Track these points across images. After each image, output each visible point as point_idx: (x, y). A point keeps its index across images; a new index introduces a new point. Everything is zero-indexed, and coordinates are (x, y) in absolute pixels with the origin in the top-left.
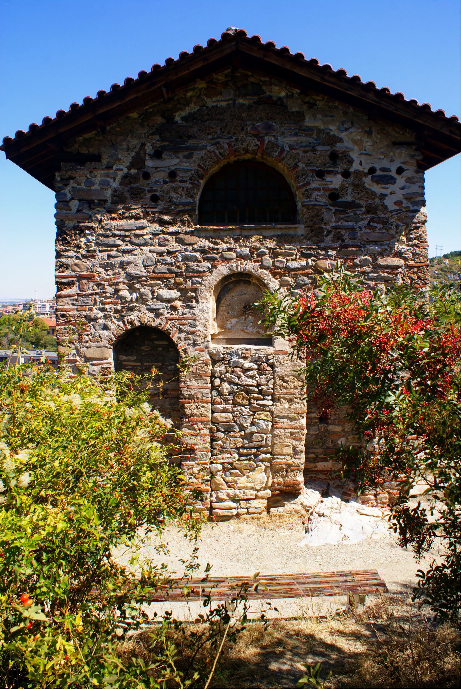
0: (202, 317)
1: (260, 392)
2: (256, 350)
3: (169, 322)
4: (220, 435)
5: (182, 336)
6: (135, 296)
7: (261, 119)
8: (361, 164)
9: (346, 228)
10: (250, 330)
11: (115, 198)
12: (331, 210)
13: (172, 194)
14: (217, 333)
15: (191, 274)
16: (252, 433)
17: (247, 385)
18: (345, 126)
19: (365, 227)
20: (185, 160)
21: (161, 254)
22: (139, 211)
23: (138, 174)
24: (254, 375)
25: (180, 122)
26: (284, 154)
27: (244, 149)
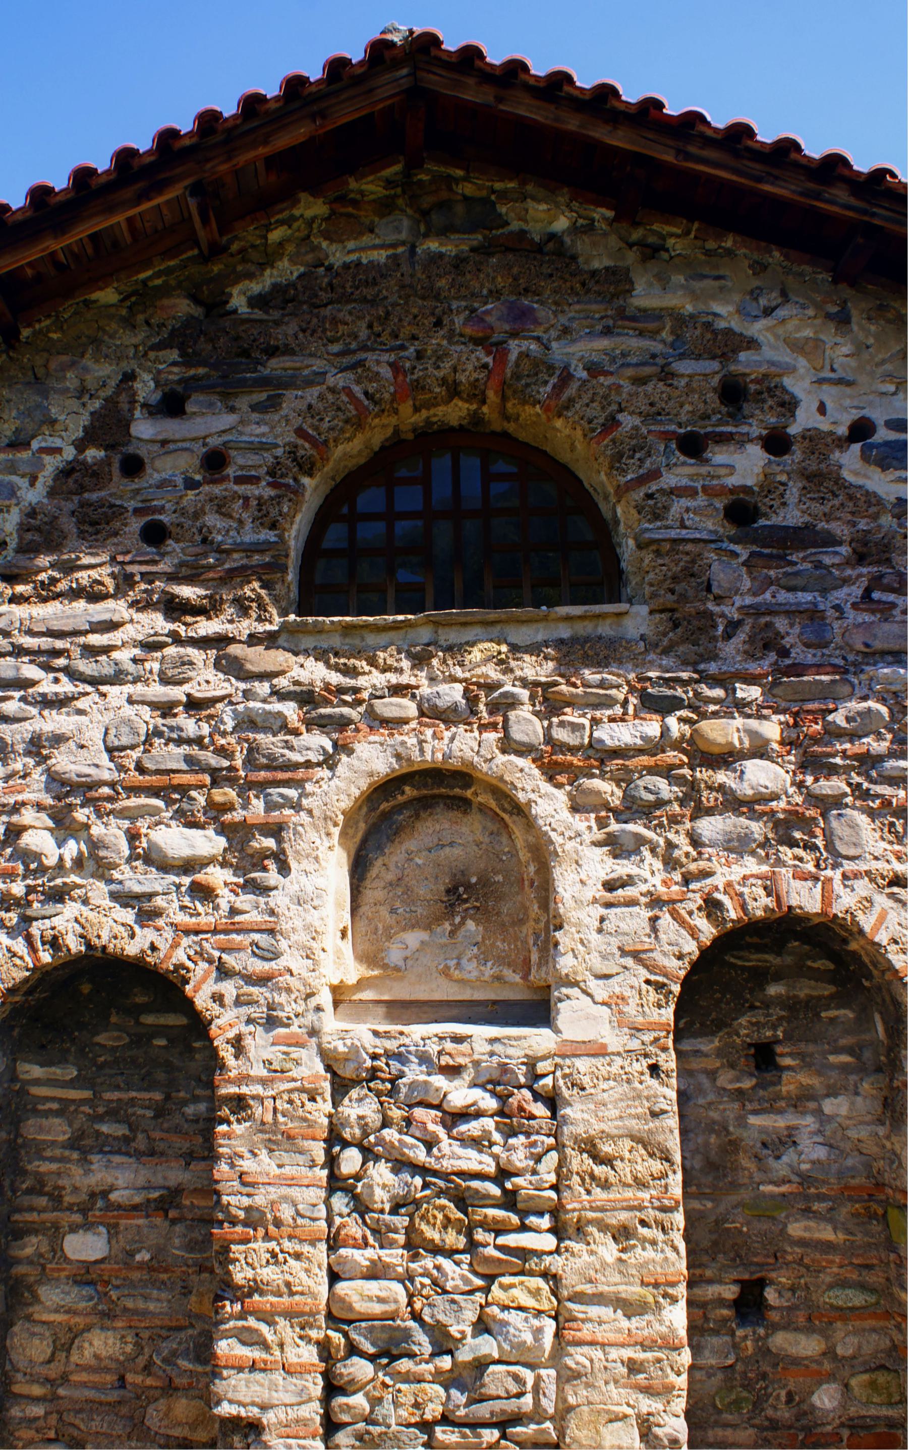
0: (298, 924)
1: (510, 1200)
2: (493, 1041)
3: (185, 941)
4: (360, 1369)
5: (229, 989)
6: (72, 849)
7: (496, 294)
8: (822, 409)
9: (791, 613)
10: (471, 970)
11: (29, 536)
12: (735, 555)
13: (211, 519)
14: (352, 980)
15: (263, 775)
16: (481, 1365)
17: (461, 1174)
18: (763, 302)
19: (855, 606)
20: (255, 416)
21: (166, 709)
22: (103, 574)
23: (107, 462)
24: (486, 1134)
25: (244, 309)
26: (571, 390)
27: (444, 381)
